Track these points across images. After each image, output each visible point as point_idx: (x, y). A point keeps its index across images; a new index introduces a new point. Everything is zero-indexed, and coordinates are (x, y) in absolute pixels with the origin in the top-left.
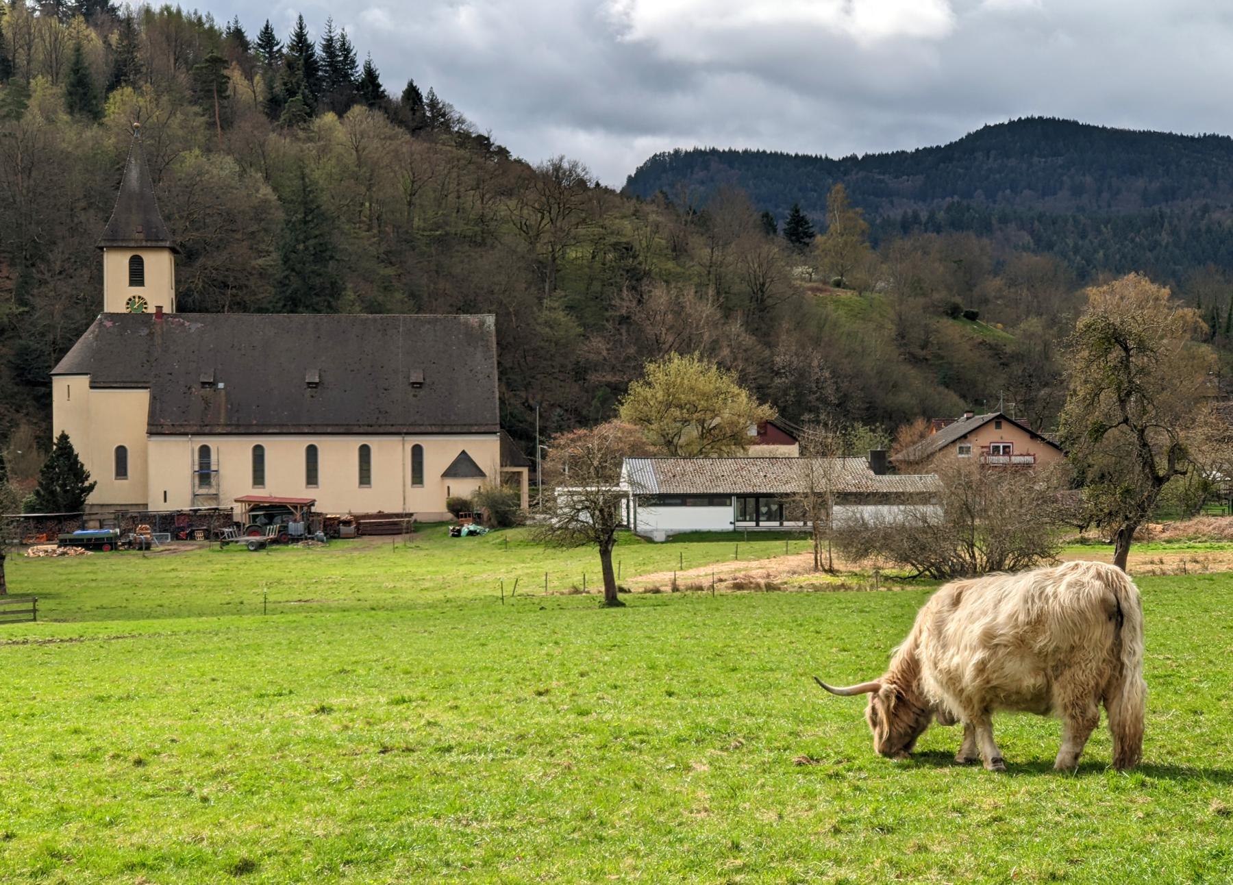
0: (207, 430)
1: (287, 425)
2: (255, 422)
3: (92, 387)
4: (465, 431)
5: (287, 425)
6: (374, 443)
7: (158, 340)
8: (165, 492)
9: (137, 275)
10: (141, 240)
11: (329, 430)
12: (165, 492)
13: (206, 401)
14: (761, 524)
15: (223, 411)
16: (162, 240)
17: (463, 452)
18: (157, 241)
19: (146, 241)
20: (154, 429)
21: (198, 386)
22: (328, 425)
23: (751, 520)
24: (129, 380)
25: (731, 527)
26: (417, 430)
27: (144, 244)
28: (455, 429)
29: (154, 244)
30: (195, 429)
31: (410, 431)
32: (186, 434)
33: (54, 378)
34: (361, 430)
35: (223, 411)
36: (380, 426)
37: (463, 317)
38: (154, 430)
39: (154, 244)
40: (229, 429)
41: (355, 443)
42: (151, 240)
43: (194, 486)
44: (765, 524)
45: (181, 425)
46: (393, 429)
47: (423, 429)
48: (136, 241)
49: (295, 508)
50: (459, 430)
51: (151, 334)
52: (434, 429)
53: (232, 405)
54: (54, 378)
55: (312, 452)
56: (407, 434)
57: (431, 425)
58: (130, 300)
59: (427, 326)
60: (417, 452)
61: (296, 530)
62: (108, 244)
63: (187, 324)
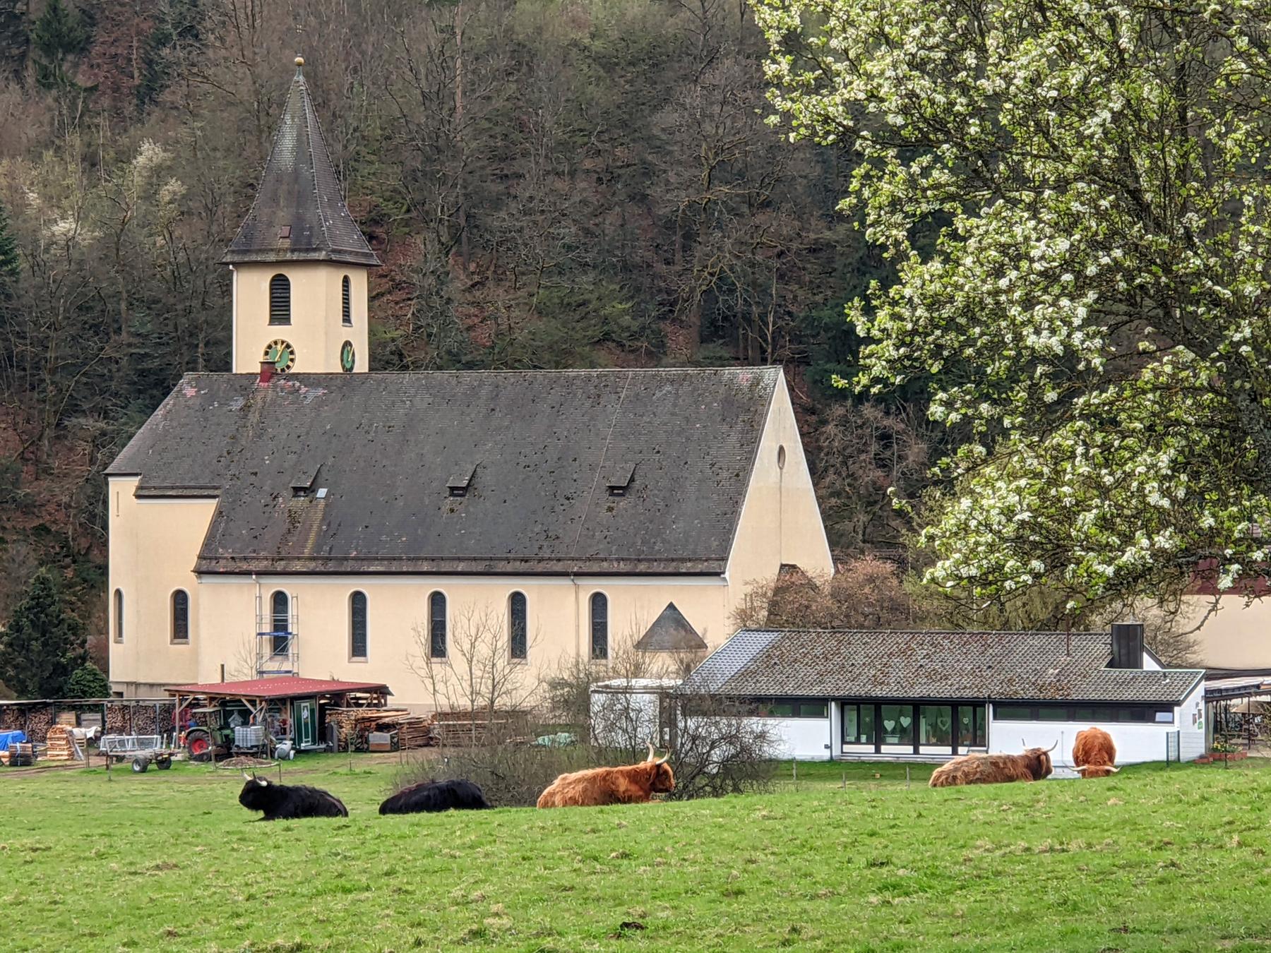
0: (280, 566)
1: (401, 559)
2: (354, 554)
3: (138, 497)
4: (670, 570)
5: (401, 559)
6: (530, 588)
7: (254, 418)
8: (223, 666)
9: (280, 310)
10: (285, 251)
11: (461, 567)
12: (223, 666)
13: (293, 518)
14: (922, 749)
15: (312, 535)
16: (315, 250)
17: (671, 606)
18: (307, 250)
19: (293, 251)
20: (205, 566)
21: (287, 493)
22: (459, 559)
23: (868, 743)
24: (192, 484)
25: (826, 755)
26: (596, 568)
27: (289, 256)
28: (656, 567)
29: (302, 256)
30: (263, 565)
31: (585, 570)
32: (248, 573)
33: (110, 479)
34: (509, 568)
35: (312, 535)
36: (540, 561)
37: (727, 372)
38: (204, 568)
39: (302, 256)
40: (312, 566)
41: (500, 591)
42: (300, 250)
43: (260, 656)
44: (894, 750)
45: (245, 559)
46: (559, 567)
47: (605, 566)
48: (278, 251)
49: (253, 703)
50: (660, 570)
51: (246, 408)
52: (623, 567)
53: (329, 525)
54: (110, 479)
55: (358, 603)
56: (577, 574)
57: (618, 560)
58: (270, 347)
59: (668, 388)
60: (599, 603)
61: (245, 739)
62: (237, 258)
63: (304, 390)
